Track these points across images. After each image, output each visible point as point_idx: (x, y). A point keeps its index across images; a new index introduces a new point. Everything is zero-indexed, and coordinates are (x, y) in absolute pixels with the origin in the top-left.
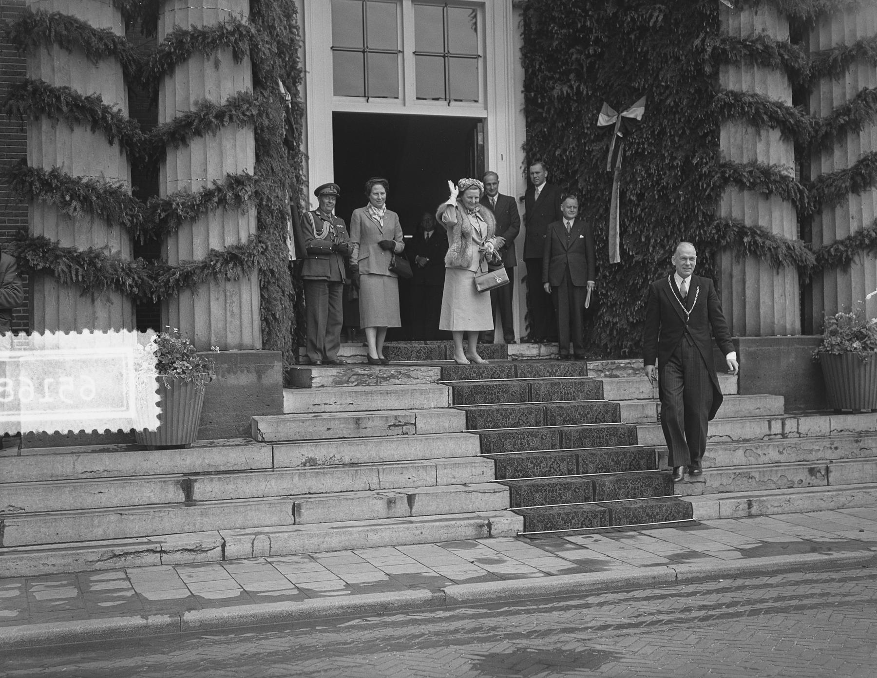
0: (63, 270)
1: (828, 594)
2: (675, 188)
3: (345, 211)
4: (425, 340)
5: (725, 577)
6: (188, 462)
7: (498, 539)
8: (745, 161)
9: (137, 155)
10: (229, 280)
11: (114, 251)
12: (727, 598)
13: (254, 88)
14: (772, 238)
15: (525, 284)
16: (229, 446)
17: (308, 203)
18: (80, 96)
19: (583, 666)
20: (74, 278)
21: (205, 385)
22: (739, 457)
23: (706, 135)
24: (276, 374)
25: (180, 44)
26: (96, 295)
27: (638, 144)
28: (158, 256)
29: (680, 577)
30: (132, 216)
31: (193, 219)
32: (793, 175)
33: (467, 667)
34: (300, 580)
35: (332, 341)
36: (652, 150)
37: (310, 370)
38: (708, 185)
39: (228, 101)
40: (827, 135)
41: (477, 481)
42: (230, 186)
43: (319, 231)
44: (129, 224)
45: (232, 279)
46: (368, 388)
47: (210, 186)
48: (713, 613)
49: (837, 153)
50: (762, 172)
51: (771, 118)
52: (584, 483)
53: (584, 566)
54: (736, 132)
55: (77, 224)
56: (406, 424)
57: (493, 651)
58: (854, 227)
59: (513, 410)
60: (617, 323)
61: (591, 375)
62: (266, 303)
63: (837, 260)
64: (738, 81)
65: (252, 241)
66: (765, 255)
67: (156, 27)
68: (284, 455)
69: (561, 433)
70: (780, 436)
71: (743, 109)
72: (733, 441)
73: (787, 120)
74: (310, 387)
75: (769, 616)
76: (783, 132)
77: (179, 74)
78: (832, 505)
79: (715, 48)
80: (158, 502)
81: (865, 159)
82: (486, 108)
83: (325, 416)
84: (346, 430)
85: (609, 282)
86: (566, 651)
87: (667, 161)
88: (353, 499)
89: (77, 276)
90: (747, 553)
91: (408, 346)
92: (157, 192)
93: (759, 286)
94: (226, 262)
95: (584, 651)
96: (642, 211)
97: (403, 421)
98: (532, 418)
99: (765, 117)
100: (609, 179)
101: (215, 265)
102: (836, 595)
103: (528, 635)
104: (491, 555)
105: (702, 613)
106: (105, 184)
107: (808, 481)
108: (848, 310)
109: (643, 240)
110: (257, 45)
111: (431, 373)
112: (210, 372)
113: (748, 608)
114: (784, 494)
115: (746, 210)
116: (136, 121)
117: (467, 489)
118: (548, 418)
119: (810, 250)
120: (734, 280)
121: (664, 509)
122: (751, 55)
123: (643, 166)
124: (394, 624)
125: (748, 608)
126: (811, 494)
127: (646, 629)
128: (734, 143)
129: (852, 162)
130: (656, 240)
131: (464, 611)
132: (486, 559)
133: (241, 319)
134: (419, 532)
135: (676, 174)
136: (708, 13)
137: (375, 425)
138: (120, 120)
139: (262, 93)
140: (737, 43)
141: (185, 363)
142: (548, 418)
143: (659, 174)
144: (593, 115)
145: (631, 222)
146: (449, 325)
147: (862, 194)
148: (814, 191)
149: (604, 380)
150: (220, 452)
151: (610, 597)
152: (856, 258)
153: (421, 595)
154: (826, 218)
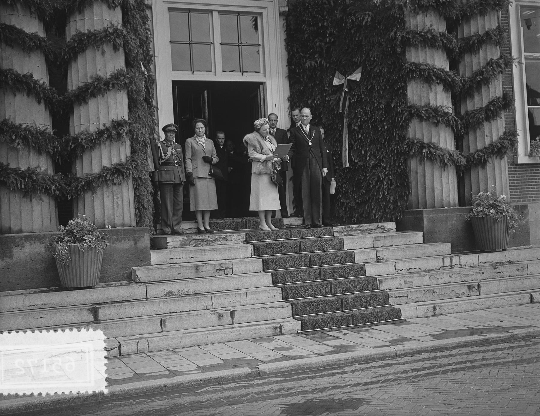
0: (12, 182)
1: (487, 359)
2: (382, 121)
3: (181, 140)
4: (233, 217)
5: (425, 351)
6: (94, 297)
7: (286, 336)
8: (423, 104)
9: (56, 110)
10: (115, 184)
11: (43, 169)
12: (427, 364)
13: (127, 67)
14: (441, 149)
15: (292, 182)
16: (119, 286)
17: (159, 136)
18: (20, 75)
19: (348, 408)
20: (19, 186)
21: (104, 249)
22: (426, 280)
23: (399, 89)
24: (145, 240)
25: (81, 41)
26: (33, 196)
27: (358, 95)
28: (70, 172)
29: (398, 353)
30: (54, 147)
31: (92, 148)
32: (451, 112)
33: (279, 412)
34: (169, 366)
35: (177, 220)
36: (367, 99)
37: (166, 238)
38: (401, 119)
39: (111, 75)
40: (470, 87)
41: (272, 301)
42: (114, 127)
43: (165, 153)
44: (52, 152)
45: (117, 184)
46: (202, 248)
47: (102, 128)
48: (421, 373)
49: (476, 98)
50: (433, 110)
51: (437, 78)
52: (336, 300)
53: (340, 349)
54: (417, 87)
55: (20, 153)
56: (226, 268)
57: (292, 402)
58: (487, 142)
59: (291, 257)
60: (348, 203)
61: (336, 235)
62: (138, 198)
63: (479, 161)
64: (416, 56)
65: (128, 161)
66: (437, 159)
67: (64, 32)
68: (153, 290)
69: (320, 270)
70: (450, 267)
71: (420, 73)
72: (422, 271)
73: (447, 79)
74: (166, 248)
75: (454, 373)
76: (444, 86)
77: (80, 60)
78: (482, 307)
79: (403, 37)
80: (77, 322)
81: (493, 101)
82: (265, 76)
83: (177, 265)
84: (190, 273)
85: (343, 179)
86: (337, 400)
87: (376, 105)
88: (197, 315)
89: (21, 185)
90: (436, 337)
91: (223, 221)
92: (68, 132)
93: (433, 178)
94: (113, 174)
95: (347, 399)
96: (362, 135)
97: (225, 267)
98: (302, 262)
99: (434, 77)
100: (341, 117)
101: (106, 175)
102: (491, 359)
103: (313, 391)
104: (283, 345)
105: (414, 374)
106: (36, 128)
107: (468, 293)
108: (486, 191)
109: (363, 153)
110: (128, 41)
111: (240, 237)
112: (106, 241)
113: (441, 369)
114: (454, 302)
115: (424, 133)
116: (54, 89)
117: (265, 306)
118: (311, 261)
119: (463, 156)
120: (419, 175)
121: (384, 313)
122: (424, 41)
123: (361, 108)
124: (230, 389)
125: (441, 369)
126: (470, 301)
127: (382, 385)
128: (416, 93)
129: (485, 104)
130: (371, 153)
131: (271, 379)
132: (280, 348)
133: (123, 208)
134: (238, 333)
135: (382, 113)
136: (398, 16)
137: (208, 270)
138: (45, 89)
139: (131, 70)
140: (415, 33)
141: (90, 236)
142: (311, 261)
143: (371, 113)
144: (330, 79)
145: (355, 142)
146: (258, 208)
147: (492, 121)
148: (464, 121)
149: (344, 237)
150: (114, 290)
151: (358, 367)
152: (490, 160)
153: (244, 371)
154: (471, 136)
